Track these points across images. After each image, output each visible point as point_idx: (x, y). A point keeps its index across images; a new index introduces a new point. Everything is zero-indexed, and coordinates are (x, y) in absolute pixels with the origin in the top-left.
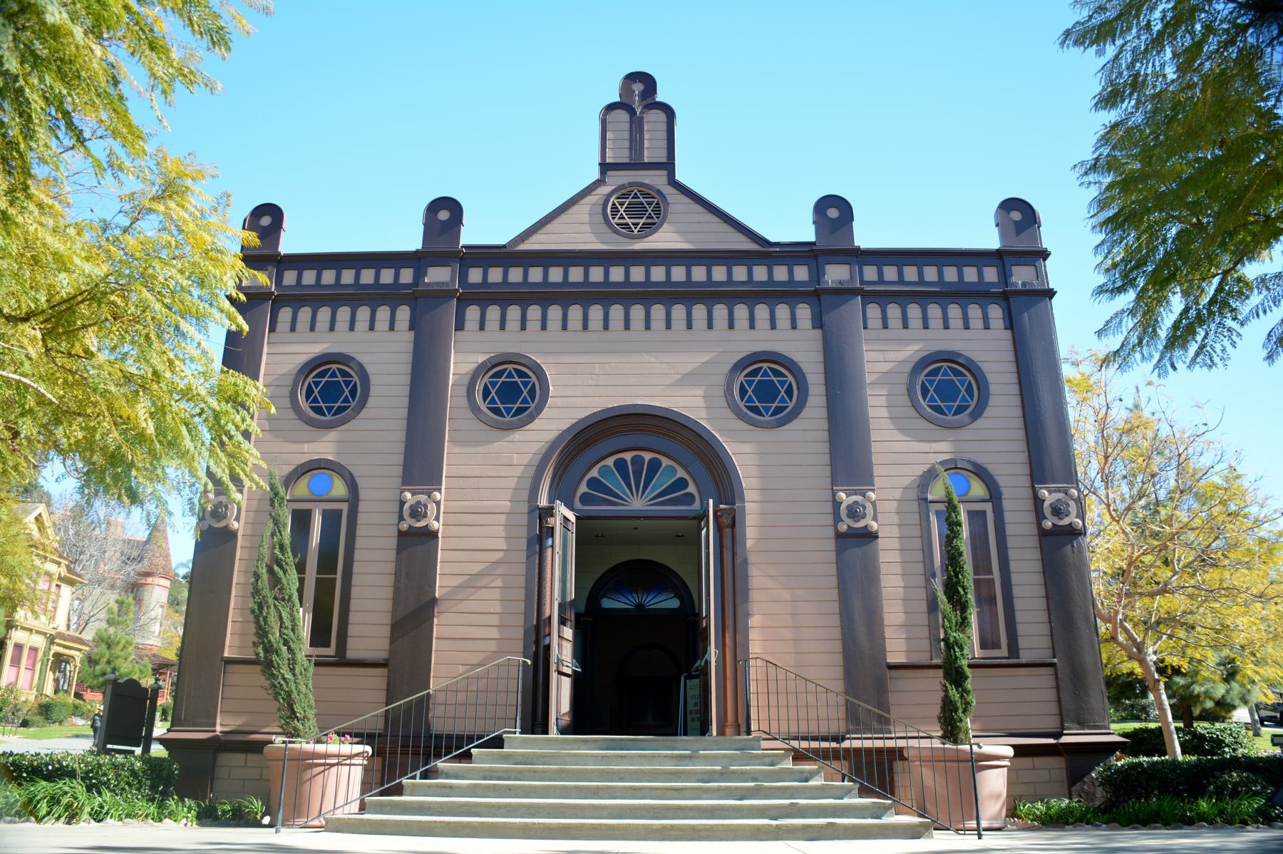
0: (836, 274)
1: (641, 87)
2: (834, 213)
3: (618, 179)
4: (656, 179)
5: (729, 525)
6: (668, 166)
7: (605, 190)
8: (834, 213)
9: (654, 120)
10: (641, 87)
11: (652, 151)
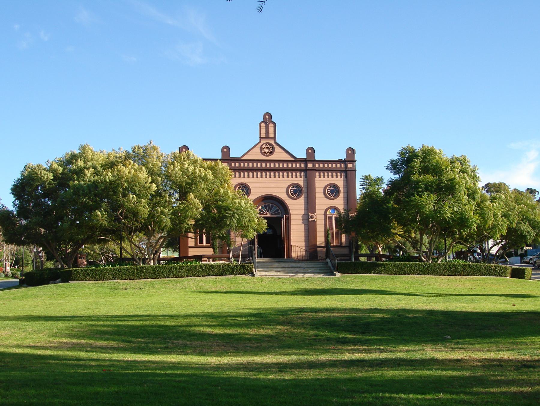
0: (310, 165)
1: (268, 119)
2: (311, 151)
3: (263, 141)
4: (272, 142)
5: (288, 220)
6: (275, 138)
7: (261, 144)
8: (311, 151)
9: (271, 126)
10: (268, 119)
11: (271, 135)
